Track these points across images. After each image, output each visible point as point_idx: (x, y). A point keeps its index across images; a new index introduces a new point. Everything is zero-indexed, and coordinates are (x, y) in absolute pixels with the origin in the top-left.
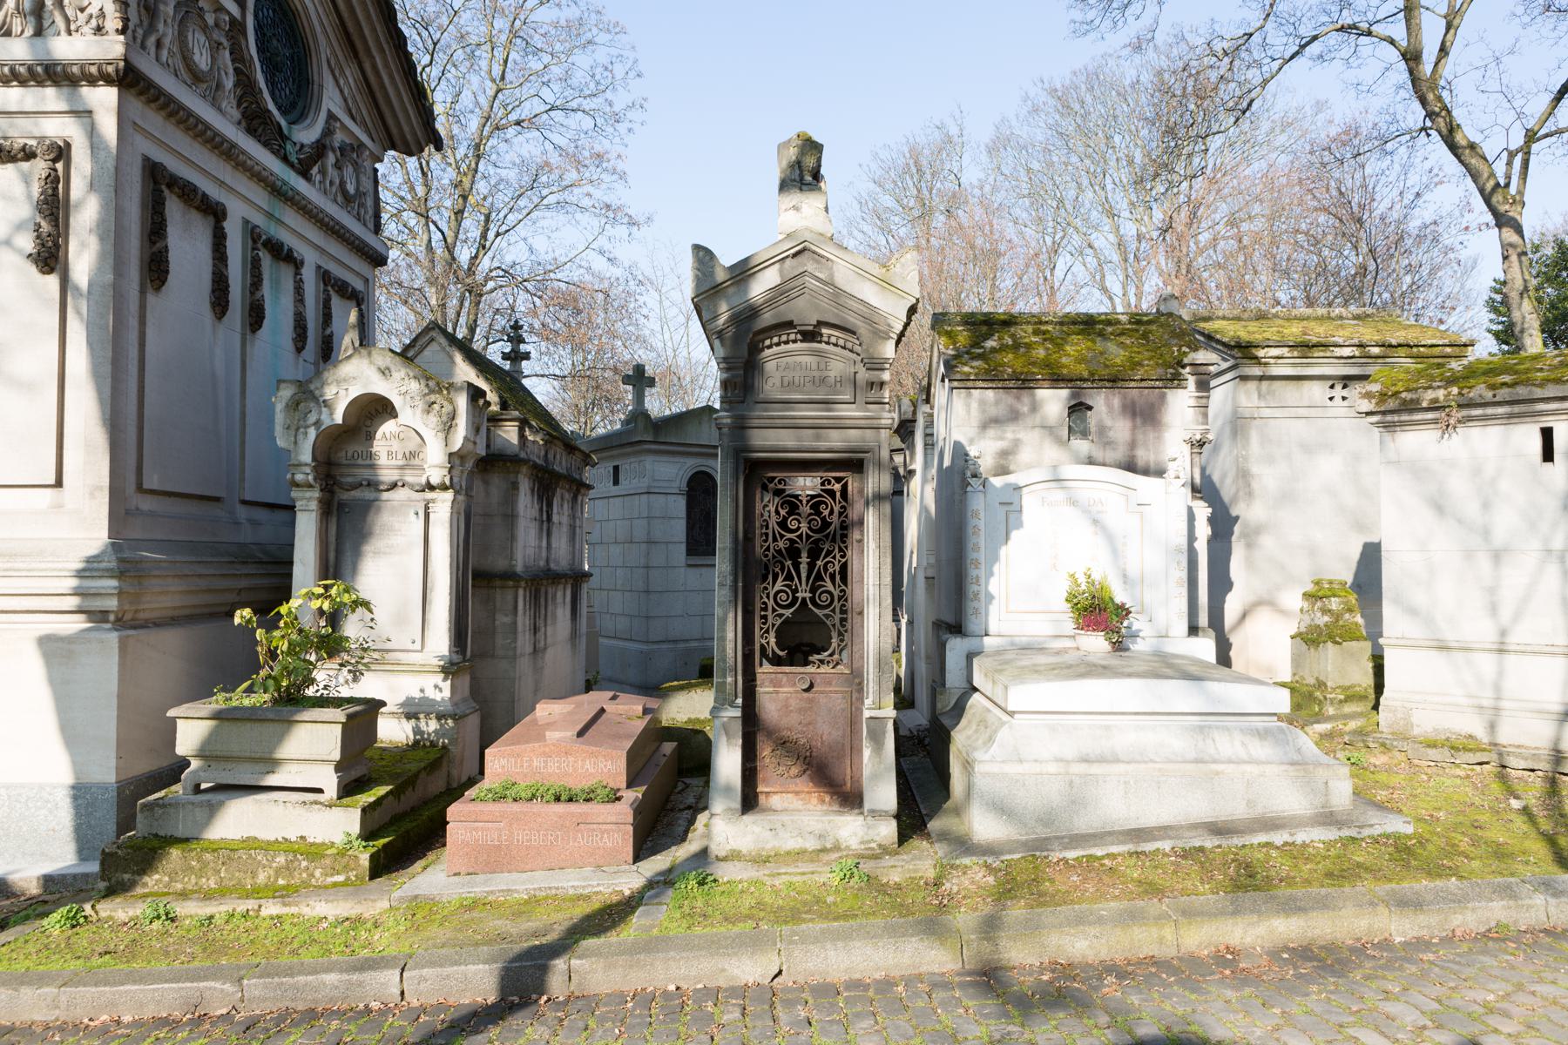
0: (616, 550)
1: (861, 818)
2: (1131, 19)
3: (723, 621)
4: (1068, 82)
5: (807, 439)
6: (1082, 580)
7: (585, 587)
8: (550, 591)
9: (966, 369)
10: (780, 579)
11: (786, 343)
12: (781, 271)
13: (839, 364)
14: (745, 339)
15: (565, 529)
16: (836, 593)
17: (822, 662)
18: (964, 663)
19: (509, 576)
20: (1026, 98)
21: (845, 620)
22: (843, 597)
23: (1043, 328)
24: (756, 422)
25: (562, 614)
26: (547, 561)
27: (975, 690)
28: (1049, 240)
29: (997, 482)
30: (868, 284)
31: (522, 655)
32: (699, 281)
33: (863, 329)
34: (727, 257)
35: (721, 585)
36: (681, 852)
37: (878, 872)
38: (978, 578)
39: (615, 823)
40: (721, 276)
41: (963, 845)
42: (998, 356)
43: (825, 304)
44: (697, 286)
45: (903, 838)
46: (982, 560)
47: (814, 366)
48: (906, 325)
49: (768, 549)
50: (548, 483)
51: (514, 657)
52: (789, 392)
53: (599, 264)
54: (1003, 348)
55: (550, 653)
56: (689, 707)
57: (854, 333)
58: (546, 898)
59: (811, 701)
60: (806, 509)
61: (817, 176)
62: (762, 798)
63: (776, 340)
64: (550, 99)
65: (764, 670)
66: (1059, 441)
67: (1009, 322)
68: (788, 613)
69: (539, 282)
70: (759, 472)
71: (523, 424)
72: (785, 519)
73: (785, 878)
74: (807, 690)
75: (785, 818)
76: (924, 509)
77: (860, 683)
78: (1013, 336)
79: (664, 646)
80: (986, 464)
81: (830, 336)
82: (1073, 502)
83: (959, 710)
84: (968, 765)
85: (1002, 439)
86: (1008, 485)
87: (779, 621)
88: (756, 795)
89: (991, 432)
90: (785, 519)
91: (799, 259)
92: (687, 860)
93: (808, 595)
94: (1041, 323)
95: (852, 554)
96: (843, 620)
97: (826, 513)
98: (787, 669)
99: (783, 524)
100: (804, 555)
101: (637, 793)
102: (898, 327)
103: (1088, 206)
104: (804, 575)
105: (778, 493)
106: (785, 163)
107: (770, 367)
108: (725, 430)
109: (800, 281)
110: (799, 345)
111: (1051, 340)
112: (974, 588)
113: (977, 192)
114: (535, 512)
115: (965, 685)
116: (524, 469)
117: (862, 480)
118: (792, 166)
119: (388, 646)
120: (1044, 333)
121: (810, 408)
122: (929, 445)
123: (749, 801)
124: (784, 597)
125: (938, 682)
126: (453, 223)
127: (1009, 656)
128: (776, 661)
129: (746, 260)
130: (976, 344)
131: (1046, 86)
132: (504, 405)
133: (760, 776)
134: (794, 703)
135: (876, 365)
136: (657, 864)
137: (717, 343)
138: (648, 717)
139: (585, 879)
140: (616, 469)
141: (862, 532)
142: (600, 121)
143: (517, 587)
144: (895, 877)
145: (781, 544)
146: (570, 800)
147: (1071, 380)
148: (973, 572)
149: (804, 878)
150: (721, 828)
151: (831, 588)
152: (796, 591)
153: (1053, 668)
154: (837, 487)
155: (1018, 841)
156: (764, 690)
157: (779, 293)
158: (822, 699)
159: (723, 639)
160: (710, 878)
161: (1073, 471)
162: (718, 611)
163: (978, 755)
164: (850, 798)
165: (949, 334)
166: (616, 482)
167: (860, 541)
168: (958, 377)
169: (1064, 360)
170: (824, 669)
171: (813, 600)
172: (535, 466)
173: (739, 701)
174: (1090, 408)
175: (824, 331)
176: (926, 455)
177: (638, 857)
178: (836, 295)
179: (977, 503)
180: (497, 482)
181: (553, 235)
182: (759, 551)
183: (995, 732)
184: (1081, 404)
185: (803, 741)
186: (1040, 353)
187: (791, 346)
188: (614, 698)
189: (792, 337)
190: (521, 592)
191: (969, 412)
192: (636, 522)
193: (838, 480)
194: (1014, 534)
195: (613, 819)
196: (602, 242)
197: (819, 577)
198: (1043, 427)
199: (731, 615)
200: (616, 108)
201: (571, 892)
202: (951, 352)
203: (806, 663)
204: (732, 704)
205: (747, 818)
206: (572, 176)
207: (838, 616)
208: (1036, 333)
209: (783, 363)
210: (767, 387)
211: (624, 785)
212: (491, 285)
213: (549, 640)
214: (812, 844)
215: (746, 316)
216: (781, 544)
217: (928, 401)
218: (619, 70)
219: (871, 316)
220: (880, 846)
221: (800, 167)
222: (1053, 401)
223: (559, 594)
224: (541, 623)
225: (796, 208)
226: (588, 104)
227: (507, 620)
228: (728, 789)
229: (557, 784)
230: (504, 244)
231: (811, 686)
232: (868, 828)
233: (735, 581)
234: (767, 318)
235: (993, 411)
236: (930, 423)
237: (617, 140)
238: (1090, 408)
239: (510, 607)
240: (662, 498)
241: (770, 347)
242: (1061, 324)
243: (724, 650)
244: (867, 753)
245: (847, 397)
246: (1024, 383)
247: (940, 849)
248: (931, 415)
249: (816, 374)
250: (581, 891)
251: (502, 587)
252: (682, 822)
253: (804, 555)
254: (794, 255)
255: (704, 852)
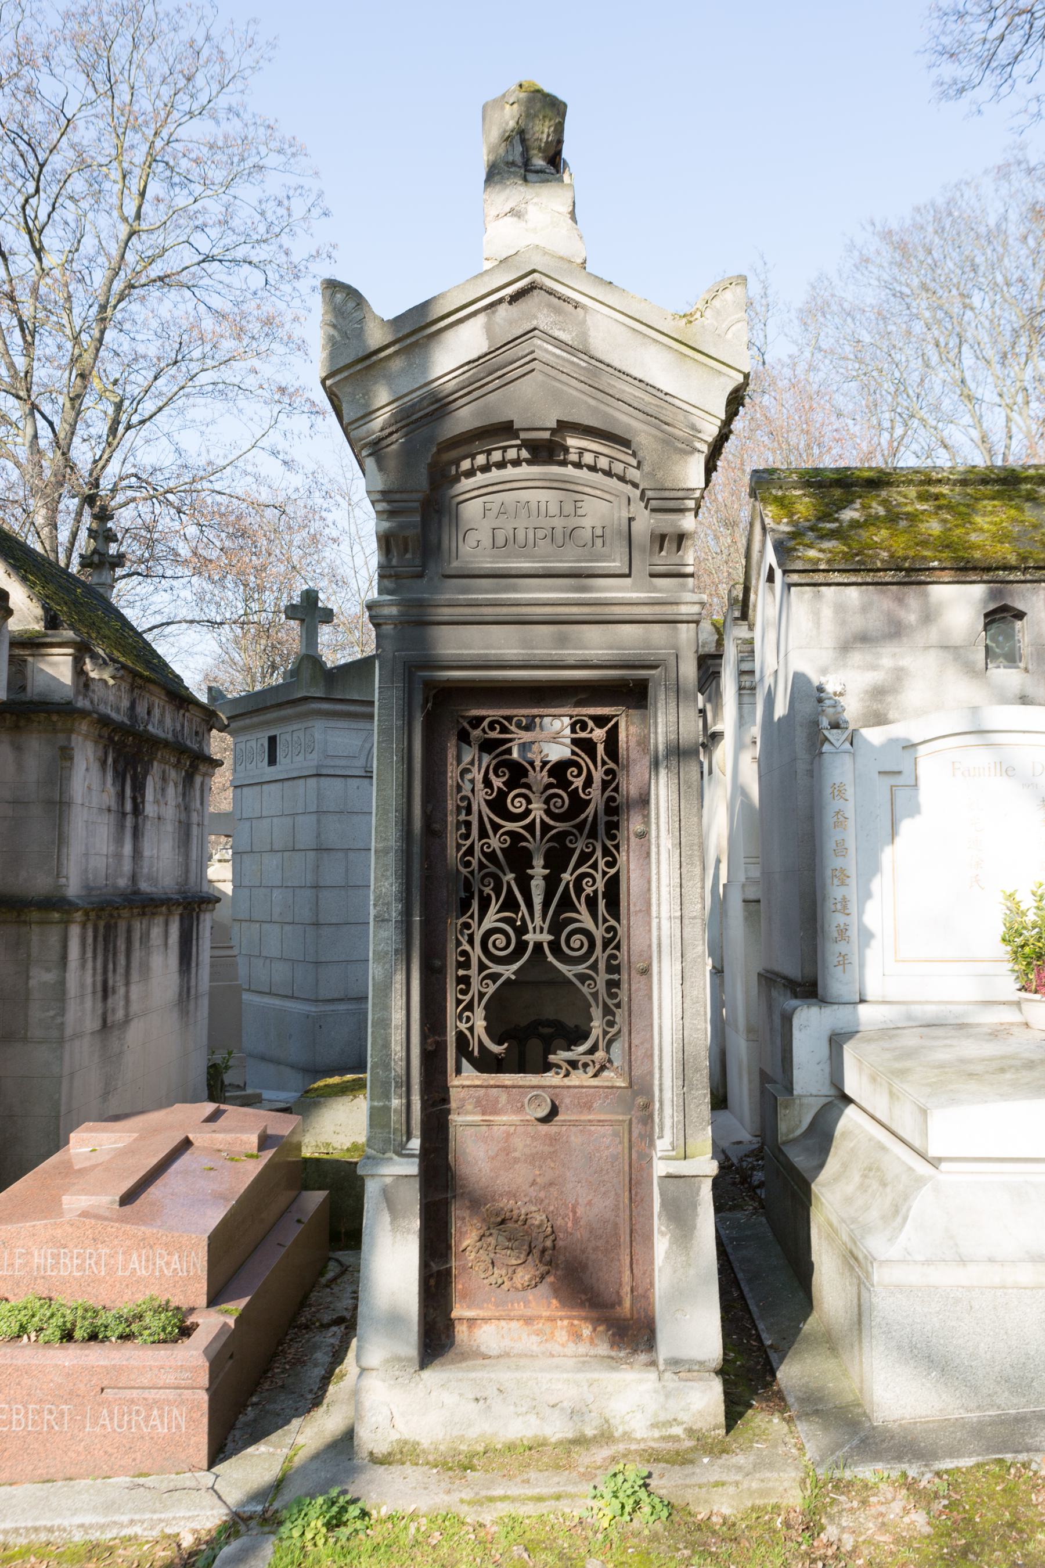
0: (271, 862)
1: (652, 1375)
2: (1021, 83)
3: (384, 989)
4: (908, 222)
5: (542, 644)
6: (1028, 903)
7: (207, 921)
8: (137, 926)
9: (812, 553)
10: (494, 908)
11: (501, 465)
12: (489, 329)
13: (603, 506)
14: (425, 462)
15: (169, 827)
16: (599, 934)
17: (573, 1064)
18: (824, 1050)
19: (55, 905)
20: (851, 247)
21: (617, 984)
22: (612, 941)
23: (934, 490)
24: (446, 613)
25: (161, 966)
26: (134, 878)
27: (848, 1100)
28: (886, 436)
29: (874, 735)
30: (653, 349)
31: (78, 1036)
32: (335, 347)
33: (643, 435)
34: (388, 302)
35: (380, 920)
36: (307, 1435)
37: (689, 1495)
38: (845, 901)
39: (176, 1381)
40: (376, 337)
41: (855, 1432)
42: (864, 534)
43: (574, 391)
44: (333, 356)
45: (735, 1410)
46: (852, 871)
47: (553, 509)
48: (727, 422)
49: (470, 851)
50: (131, 753)
51: (61, 1041)
52: (508, 556)
53: (271, 468)
54: (871, 521)
55: (135, 1033)
56: (340, 1128)
57: (625, 443)
58: (28, 1550)
59: (553, 1140)
60: (540, 778)
61: (555, 160)
62: (461, 1331)
63: (481, 460)
64: (205, 249)
65: (465, 1082)
66: (969, 670)
67: (878, 482)
68: (508, 971)
69: (184, 495)
70: (447, 708)
71: (82, 651)
72: (502, 795)
73: (504, 1509)
74: (546, 1120)
75: (504, 1376)
76: (739, 790)
77: (647, 1106)
78: (885, 503)
79: (342, 1007)
80: (852, 708)
81: (582, 451)
82: (1008, 770)
83: (821, 1136)
84: (854, 1262)
85: (874, 667)
86: (892, 742)
87: (491, 989)
88: (450, 1325)
89: (857, 657)
90: (502, 795)
91: (523, 305)
92: (316, 1457)
93: (546, 937)
94: (929, 482)
95: (629, 861)
96: (613, 985)
97: (579, 783)
98: (507, 1079)
99: (498, 805)
100: (538, 862)
101: (213, 1323)
102: (711, 430)
103: (938, 389)
104: (538, 900)
105: (487, 746)
106: (495, 135)
107: (471, 510)
108: (388, 629)
109: (525, 348)
110: (525, 470)
111: (949, 508)
112: (839, 919)
113: (787, 372)
114: (109, 797)
115: (827, 1090)
116: (84, 727)
117: (644, 720)
118: (508, 139)
119: (135, 976)
120: (937, 497)
121: (543, 579)
122: (746, 690)
123: (436, 1337)
124: (501, 941)
125: (775, 1079)
126: (70, 415)
127: (910, 1040)
128: (487, 1063)
129: (424, 307)
130: (826, 516)
131: (879, 227)
132: (52, 622)
133: (458, 1286)
134: (521, 1145)
135: (667, 502)
136: (258, 1465)
137: (370, 463)
138: (269, 1154)
139: (109, 1507)
140: (272, 741)
141: (646, 817)
142: (273, 277)
143: (66, 923)
144: (723, 1506)
145: (495, 843)
146: (93, 1337)
147: (988, 569)
148: (836, 892)
149: (543, 1508)
150: (381, 1393)
151: (588, 923)
152: (522, 930)
153: (1002, 1067)
154: (599, 734)
155: (961, 1424)
156: (465, 1121)
157: (488, 370)
158: (576, 1139)
159: (384, 1023)
160: (353, 1511)
161: (1005, 716)
162: (375, 971)
163: (876, 1245)
164: (631, 1331)
165: (781, 502)
166: (272, 761)
167: (643, 835)
168: (799, 565)
169: (973, 537)
170: (577, 1078)
171: (555, 947)
172: (104, 721)
173: (415, 1144)
174: (1020, 615)
175: (572, 442)
176: (740, 704)
177: (220, 1450)
178: (594, 372)
179: (840, 771)
180: (37, 747)
181: (207, 431)
182: (453, 855)
183: (906, 1197)
184: (1004, 609)
185: (538, 1218)
186: (934, 527)
187: (510, 472)
188: (213, 1117)
189: (512, 454)
190: (75, 931)
191: (818, 624)
192: (300, 819)
193: (600, 721)
194: (906, 826)
195: (170, 1379)
196: (274, 438)
197: (566, 904)
198: (946, 648)
199: (399, 978)
200: (295, 258)
201: (78, 1537)
202: (785, 528)
203: (547, 1067)
204: (401, 1151)
205: (431, 1376)
206: (228, 345)
207: (602, 977)
208: (922, 497)
209: (496, 504)
210: (466, 549)
211: (203, 1300)
212: (120, 498)
213: (134, 1008)
214: (556, 1429)
215: (426, 412)
216: (495, 843)
217: (744, 616)
218: (299, 207)
219: (658, 408)
220: (690, 1432)
221: (523, 141)
222: (960, 604)
223: (156, 932)
224: (117, 980)
225: (515, 213)
226: (259, 254)
227: (50, 977)
228: (394, 1320)
229: (70, 1300)
230: (139, 442)
231: (554, 1111)
232: (669, 1394)
233: (407, 913)
234: (465, 417)
235: (857, 623)
236: (748, 651)
237: (297, 302)
238: (1020, 615)
239: (54, 955)
240: (338, 783)
241: (470, 473)
242: (964, 482)
243: (386, 1045)
244: (662, 1244)
245: (617, 565)
246: (910, 574)
247: (809, 1440)
248: (750, 642)
249: (558, 523)
250: (95, 1536)
251: (42, 923)
252: (322, 1357)
253: (538, 862)
254: (514, 298)
255: (344, 1444)
